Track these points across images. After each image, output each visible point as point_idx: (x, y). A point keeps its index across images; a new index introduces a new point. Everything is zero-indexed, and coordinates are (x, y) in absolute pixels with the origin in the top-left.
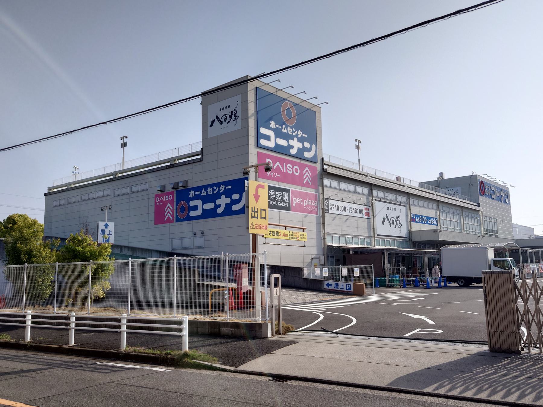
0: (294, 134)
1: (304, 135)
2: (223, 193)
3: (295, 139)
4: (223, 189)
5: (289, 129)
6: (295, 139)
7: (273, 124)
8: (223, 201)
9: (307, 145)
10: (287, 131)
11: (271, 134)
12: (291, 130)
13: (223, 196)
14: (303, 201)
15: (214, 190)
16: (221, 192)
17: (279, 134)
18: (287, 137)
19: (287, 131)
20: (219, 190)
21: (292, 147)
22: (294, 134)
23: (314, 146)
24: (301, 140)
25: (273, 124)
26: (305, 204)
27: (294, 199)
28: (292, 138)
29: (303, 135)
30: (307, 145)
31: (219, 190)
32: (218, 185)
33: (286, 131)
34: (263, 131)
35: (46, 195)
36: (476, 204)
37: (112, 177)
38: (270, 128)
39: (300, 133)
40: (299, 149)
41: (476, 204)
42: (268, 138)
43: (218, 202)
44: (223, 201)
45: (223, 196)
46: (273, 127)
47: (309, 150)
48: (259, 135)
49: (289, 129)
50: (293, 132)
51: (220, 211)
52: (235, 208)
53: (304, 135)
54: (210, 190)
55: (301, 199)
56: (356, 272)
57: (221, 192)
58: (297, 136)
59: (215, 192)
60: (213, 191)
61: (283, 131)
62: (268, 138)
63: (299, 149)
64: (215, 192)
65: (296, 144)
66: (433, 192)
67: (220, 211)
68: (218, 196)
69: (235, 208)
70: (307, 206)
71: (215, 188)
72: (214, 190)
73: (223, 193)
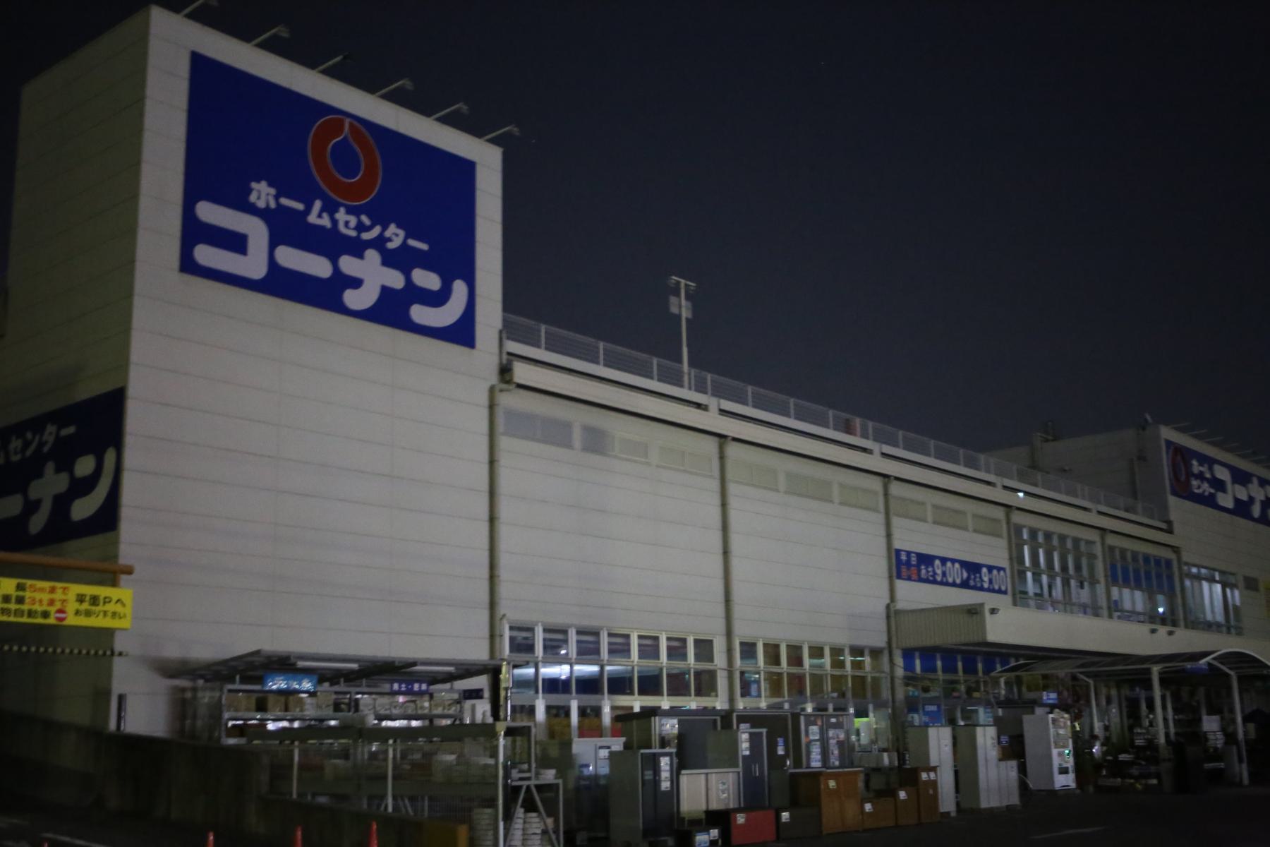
3: (372, 255)
5: (341, 216)
6: (372, 255)
11: (256, 231)
12: (353, 221)
13: (50, 467)
15: (27, 444)
16: (46, 449)
17: (286, 230)
18: (330, 244)
19: (335, 222)
21: (356, 283)
22: (366, 236)
23: (459, 288)
24: (397, 259)
25: (262, 194)
28: (357, 248)
30: (427, 280)
31: (41, 444)
32: (37, 424)
33: (326, 222)
34: (209, 212)
35: (1015, 604)
36: (1164, 526)
37: (1041, 551)
38: (252, 210)
39: (396, 236)
40: (386, 291)
41: (1164, 526)
42: (236, 243)
44: (51, 484)
45: (50, 467)
46: (261, 204)
47: (438, 299)
48: (194, 232)
49: (341, 216)
50: (361, 228)
51: (37, 523)
52: (83, 509)
54: (16, 444)
56: (309, 798)
57: (46, 449)
58: (379, 243)
59: (29, 453)
61: (312, 219)
62: (236, 243)
63: (386, 291)
64: (29, 453)
66: (990, 477)
67: (37, 523)
68: (32, 468)
69: (83, 509)
71: (29, 435)
72: (27, 444)
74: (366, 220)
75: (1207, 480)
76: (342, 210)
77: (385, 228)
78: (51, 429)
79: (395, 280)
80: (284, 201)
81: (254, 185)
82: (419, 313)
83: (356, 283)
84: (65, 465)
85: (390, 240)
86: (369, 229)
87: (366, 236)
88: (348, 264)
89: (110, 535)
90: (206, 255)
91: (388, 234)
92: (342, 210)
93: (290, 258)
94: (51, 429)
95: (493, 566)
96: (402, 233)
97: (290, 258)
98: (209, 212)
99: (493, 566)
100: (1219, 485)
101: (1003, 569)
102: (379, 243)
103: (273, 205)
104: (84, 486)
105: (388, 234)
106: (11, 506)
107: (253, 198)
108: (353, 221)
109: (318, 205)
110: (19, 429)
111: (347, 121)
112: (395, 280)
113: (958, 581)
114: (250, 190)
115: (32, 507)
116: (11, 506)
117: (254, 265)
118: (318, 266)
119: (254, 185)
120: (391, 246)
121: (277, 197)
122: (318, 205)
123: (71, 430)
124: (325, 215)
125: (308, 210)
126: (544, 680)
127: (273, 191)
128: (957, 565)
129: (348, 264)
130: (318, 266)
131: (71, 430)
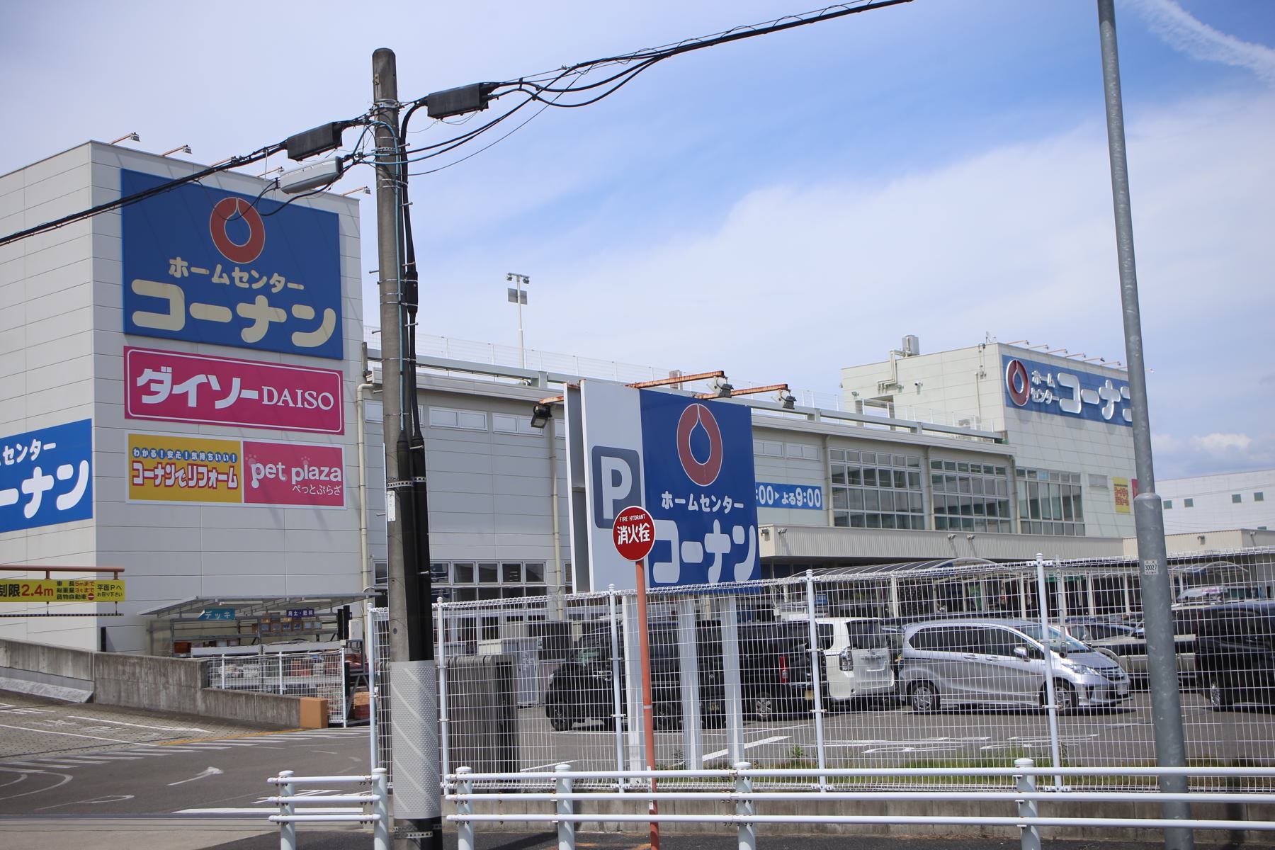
0: (715, 509)
1: (737, 505)
2: (36, 463)
3: (262, 300)
4: (37, 452)
5: (237, 274)
6: (262, 300)
7: (179, 267)
8: (38, 484)
9: (304, 312)
10: (700, 505)
11: (175, 295)
12: (246, 276)
13: (38, 471)
14: (287, 472)
15: (17, 453)
16: (33, 458)
17: (196, 290)
18: (230, 296)
19: (232, 279)
20: (29, 455)
21: (250, 323)
22: (255, 286)
23: (329, 314)
25: (179, 267)
26: (294, 479)
27: (254, 467)
29: (290, 285)
30: (304, 312)
31: (29, 455)
32: (26, 439)
33: (696, 508)
34: (142, 287)
38: (172, 280)
39: (278, 282)
40: (272, 325)
42: (161, 306)
43: (27, 486)
44: (38, 484)
45: (38, 471)
46: (178, 275)
49: (237, 274)
50: (252, 280)
51: (30, 510)
52: (66, 502)
53: (737, 505)
55: (280, 466)
57: (33, 458)
58: (266, 290)
59: (19, 460)
60: (15, 457)
62: (161, 306)
63: (272, 325)
64: (19, 460)
65: (262, 315)
67: (30, 510)
68: (25, 470)
69: (66, 502)
70: (305, 482)
71: (19, 447)
72: (17, 453)
73: (36, 463)
74: (256, 275)
75: (1051, 389)
76: (237, 269)
77: (269, 279)
78: (36, 444)
79: (280, 316)
80: (194, 270)
81: (172, 261)
82: (300, 339)
83: (250, 323)
84: (49, 470)
85: (274, 286)
86: (257, 281)
87: (255, 286)
88: (244, 310)
89: (1246, 833)
90: (142, 319)
91: (272, 282)
92: (237, 269)
93: (202, 311)
94: (36, 444)
95: (498, 120)
96: (283, 279)
97: (202, 311)
98: (142, 287)
99: (498, 120)
100: (1068, 392)
101: (819, 488)
102: (266, 290)
103: (186, 274)
104: (65, 487)
105: (272, 282)
106: (8, 497)
107: (172, 271)
108: (246, 276)
109: (219, 268)
110: (11, 441)
111: (237, 200)
112: (280, 316)
113: (771, 502)
114: (169, 265)
115: (25, 499)
116: (8, 497)
117: (174, 321)
118: (220, 314)
119: (172, 261)
120: (274, 290)
121: (188, 268)
122: (219, 268)
123: (52, 446)
124: (225, 275)
125: (212, 274)
126: (91, 517)
127: (186, 264)
128: (769, 488)
129: (244, 310)
130: (220, 314)
131: (52, 446)
